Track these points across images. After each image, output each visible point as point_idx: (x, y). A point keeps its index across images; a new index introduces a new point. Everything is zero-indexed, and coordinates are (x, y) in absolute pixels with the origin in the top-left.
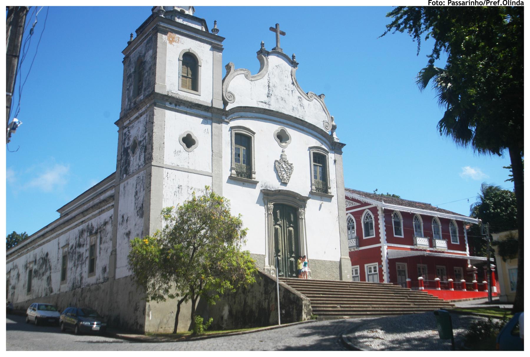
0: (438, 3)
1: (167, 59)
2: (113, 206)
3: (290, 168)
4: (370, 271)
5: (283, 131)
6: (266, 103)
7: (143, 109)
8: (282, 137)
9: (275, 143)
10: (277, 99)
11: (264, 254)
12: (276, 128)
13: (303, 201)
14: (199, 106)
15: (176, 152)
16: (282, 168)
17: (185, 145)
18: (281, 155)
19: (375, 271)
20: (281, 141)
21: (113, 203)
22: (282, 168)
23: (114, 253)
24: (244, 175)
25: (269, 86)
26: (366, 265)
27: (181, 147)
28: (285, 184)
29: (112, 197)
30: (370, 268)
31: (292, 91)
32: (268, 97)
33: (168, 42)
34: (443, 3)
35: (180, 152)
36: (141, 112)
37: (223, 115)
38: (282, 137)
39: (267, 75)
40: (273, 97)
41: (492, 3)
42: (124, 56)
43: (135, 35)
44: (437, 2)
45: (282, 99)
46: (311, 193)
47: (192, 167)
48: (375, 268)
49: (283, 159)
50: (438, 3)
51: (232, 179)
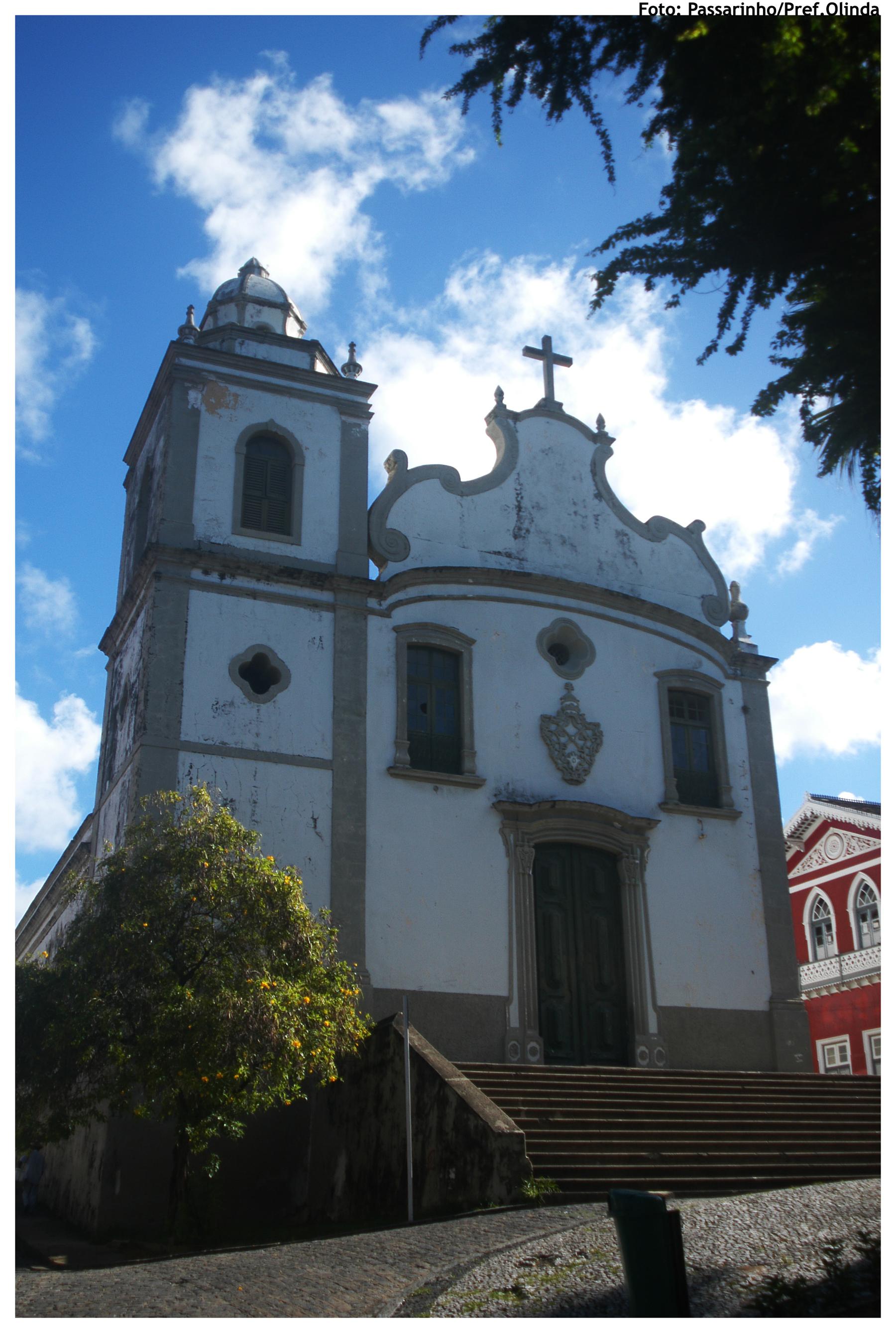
1: (202, 452)
4: (832, 1060)
5: (568, 627)
6: (509, 555)
8: (564, 651)
9: (544, 669)
10: (548, 542)
11: (504, 993)
13: (641, 827)
14: (292, 572)
15: (218, 708)
16: (569, 735)
18: (564, 699)
19: (843, 1058)
22: (569, 735)
24: (437, 747)
25: (519, 508)
26: (819, 1043)
27: (234, 691)
28: (574, 778)
30: (831, 1051)
31: (596, 517)
32: (516, 537)
33: (203, 408)
35: (232, 704)
37: (370, 594)
38: (564, 651)
39: (513, 476)
40: (532, 538)
45: (564, 542)
47: (266, 747)
48: (842, 1049)
51: (393, 771)
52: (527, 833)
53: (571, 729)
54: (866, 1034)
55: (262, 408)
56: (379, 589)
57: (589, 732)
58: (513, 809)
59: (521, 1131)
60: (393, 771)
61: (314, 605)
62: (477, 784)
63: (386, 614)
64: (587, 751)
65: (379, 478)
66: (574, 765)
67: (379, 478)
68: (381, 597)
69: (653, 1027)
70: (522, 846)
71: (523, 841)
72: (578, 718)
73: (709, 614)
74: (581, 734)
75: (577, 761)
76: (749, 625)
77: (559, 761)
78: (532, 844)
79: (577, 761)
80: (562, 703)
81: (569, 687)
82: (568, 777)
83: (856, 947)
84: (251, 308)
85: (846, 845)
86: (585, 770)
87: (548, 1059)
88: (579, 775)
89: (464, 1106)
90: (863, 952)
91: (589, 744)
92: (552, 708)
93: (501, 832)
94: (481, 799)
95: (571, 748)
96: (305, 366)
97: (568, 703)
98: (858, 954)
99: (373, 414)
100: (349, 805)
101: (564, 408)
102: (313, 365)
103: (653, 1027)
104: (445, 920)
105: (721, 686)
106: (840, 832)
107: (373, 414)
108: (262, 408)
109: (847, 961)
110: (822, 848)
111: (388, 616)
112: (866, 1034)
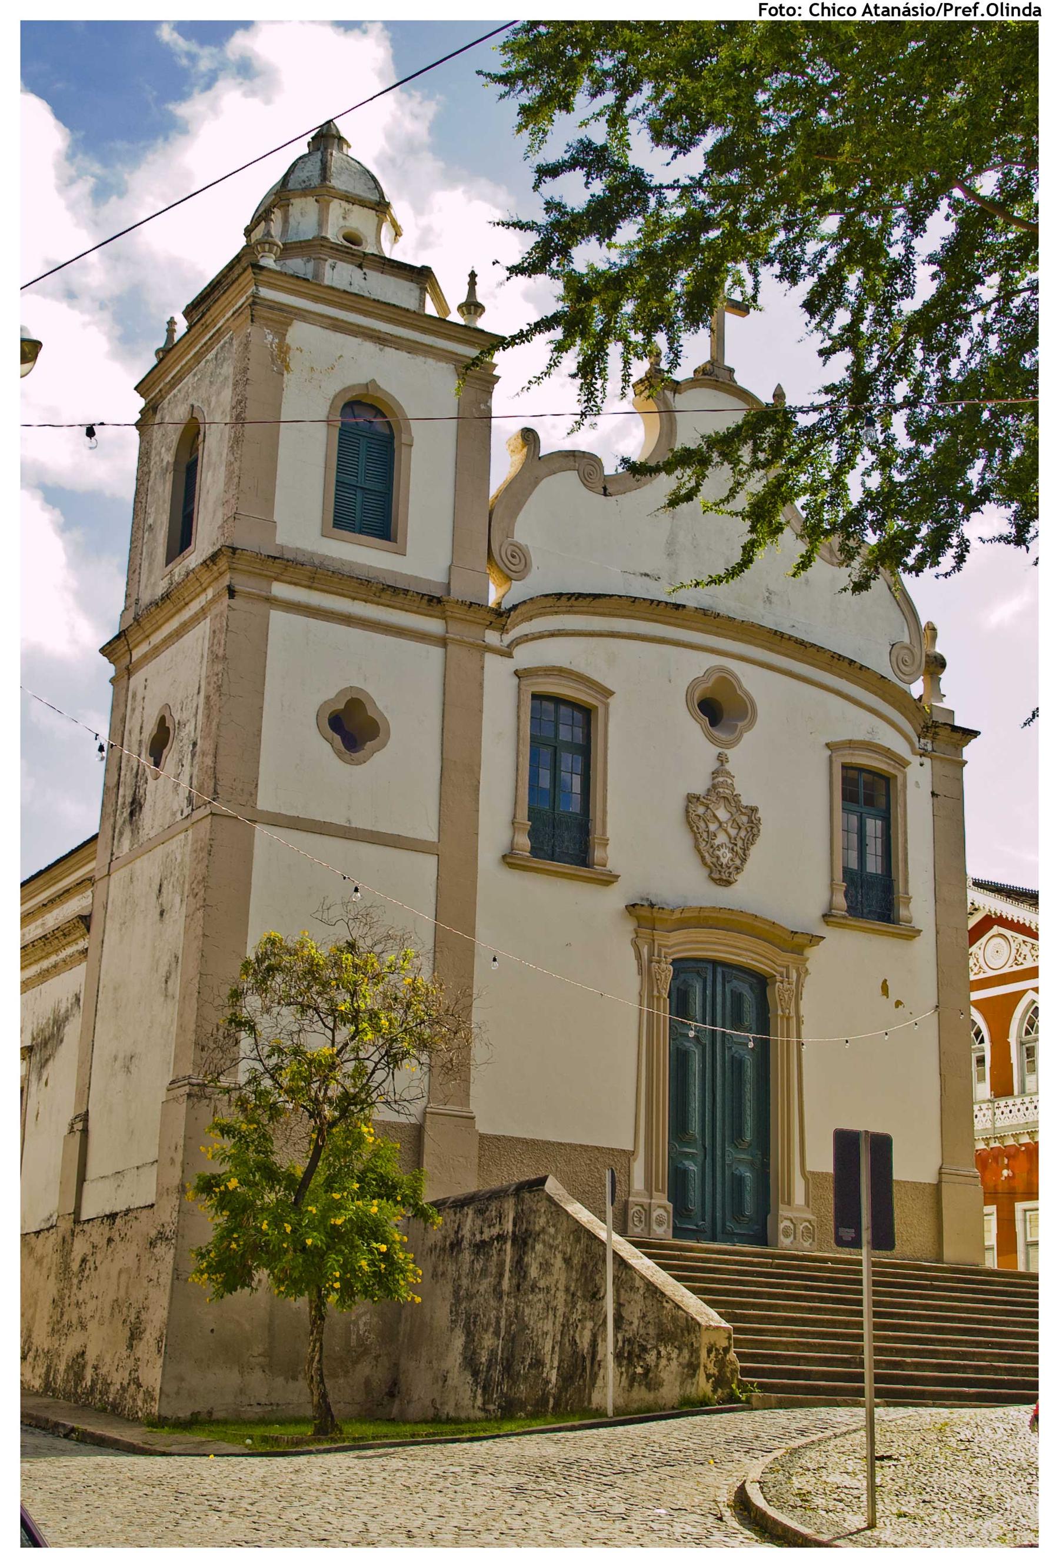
0: (784, 11)
2: (85, 952)
3: (750, 823)
5: (726, 682)
7: (195, 607)
8: (719, 709)
9: (692, 729)
11: (629, 1147)
12: (692, 666)
13: (797, 944)
17: (337, 738)
18: (715, 773)
20: (714, 723)
21: (82, 944)
23: (79, 1126)
24: (562, 835)
27: (322, 749)
28: (722, 876)
29: (85, 920)
32: (670, 555)
34: (798, 11)
36: (187, 614)
41: (960, 11)
42: (141, 403)
43: (182, 326)
44: (781, 7)
46: (827, 917)
49: (719, 788)
50: (784, 11)
51: (510, 860)
52: (666, 946)
53: (722, 814)
54: (1019, 1206)
55: (365, 364)
56: (501, 617)
57: (745, 819)
58: (644, 914)
59: (728, 1325)
60: (510, 860)
61: (422, 637)
62: (608, 880)
63: (507, 653)
64: (740, 843)
65: (503, 465)
66: (724, 861)
67: (503, 465)
68: (503, 630)
69: (799, 1198)
70: (659, 962)
71: (659, 956)
72: (732, 801)
73: (898, 664)
74: (734, 820)
75: (729, 855)
76: (946, 679)
77: (706, 855)
78: (670, 960)
79: (729, 855)
80: (714, 779)
81: (722, 759)
82: (716, 876)
83: (1016, 1092)
84: (336, 208)
85: (1014, 951)
86: (737, 868)
87: (678, 1232)
88: (730, 873)
89: (653, 1291)
90: (1027, 1099)
91: (743, 834)
92: (700, 788)
93: (635, 944)
94: (615, 899)
95: (721, 838)
96: (412, 304)
97: (721, 779)
98: (1019, 1101)
99: (499, 377)
100: (455, 903)
101: (737, 376)
102: (422, 302)
103: (799, 1198)
104: (563, 1053)
105: (903, 763)
106: (1008, 933)
107: (499, 377)
108: (365, 364)
109: (1002, 1109)
110: (981, 953)
111: (510, 655)
112: (1019, 1206)
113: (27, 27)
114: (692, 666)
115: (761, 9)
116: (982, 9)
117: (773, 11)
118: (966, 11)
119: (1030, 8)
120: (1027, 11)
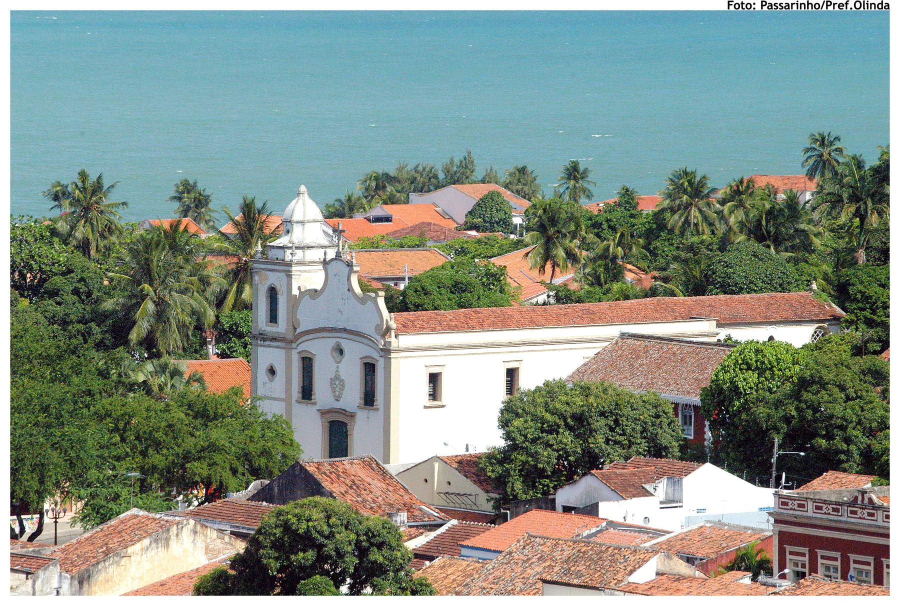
0: (744, 6)
24: (307, 393)
34: (753, 6)
41: (836, 6)
44: (742, 3)
50: (744, 6)
58: (323, 413)
60: (298, 402)
113: (12, 12)
114: (332, 342)
115: (729, 5)
116: (851, 5)
117: (737, 6)
118: (840, 6)
119: (882, 4)
120: (880, 6)
